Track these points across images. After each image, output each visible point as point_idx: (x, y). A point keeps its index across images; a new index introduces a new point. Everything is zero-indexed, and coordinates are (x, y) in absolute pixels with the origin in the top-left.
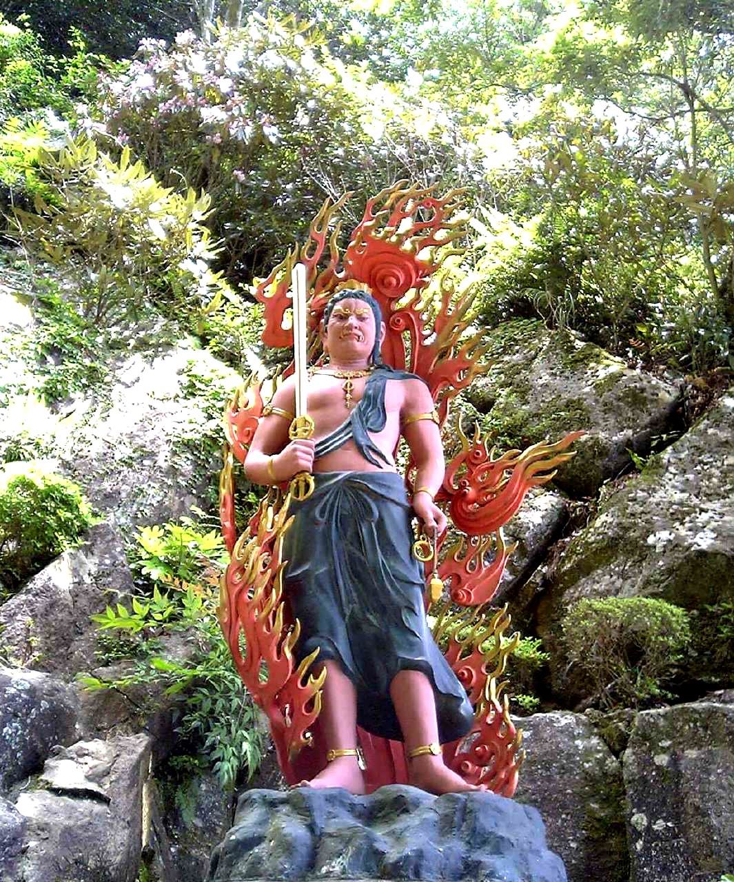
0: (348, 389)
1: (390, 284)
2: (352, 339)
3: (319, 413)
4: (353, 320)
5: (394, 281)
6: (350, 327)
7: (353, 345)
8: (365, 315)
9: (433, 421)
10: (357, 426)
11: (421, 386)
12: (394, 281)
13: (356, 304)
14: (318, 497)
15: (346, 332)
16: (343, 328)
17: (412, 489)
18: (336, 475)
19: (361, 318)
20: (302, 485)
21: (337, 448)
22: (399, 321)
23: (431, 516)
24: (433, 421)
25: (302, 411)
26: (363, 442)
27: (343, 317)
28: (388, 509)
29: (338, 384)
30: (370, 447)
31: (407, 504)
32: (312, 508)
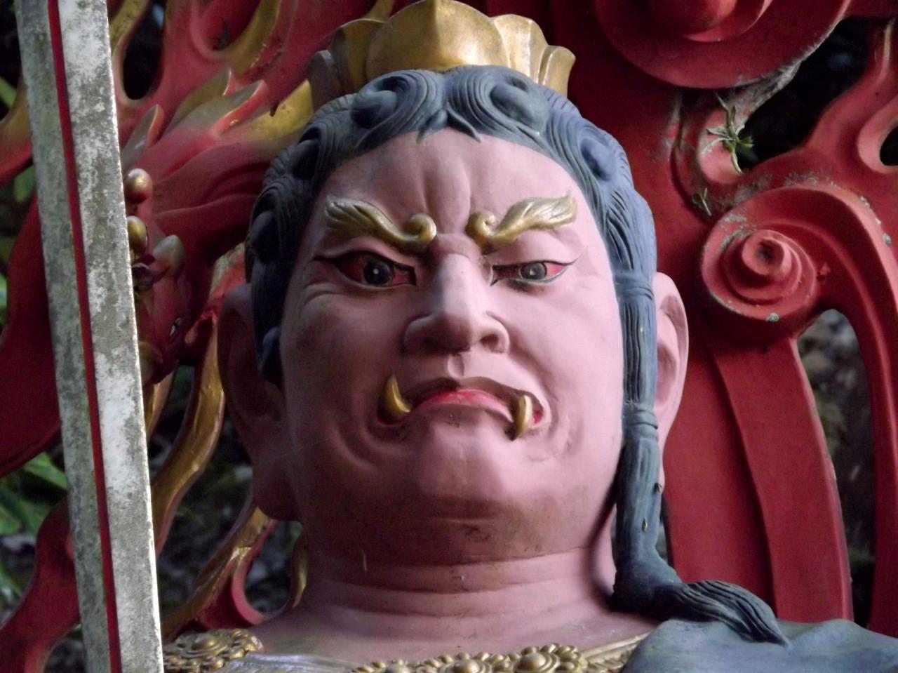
2: (465, 417)
7: (476, 464)
8: (546, 247)
13: (480, 172)
19: (515, 269)
22: (770, 253)
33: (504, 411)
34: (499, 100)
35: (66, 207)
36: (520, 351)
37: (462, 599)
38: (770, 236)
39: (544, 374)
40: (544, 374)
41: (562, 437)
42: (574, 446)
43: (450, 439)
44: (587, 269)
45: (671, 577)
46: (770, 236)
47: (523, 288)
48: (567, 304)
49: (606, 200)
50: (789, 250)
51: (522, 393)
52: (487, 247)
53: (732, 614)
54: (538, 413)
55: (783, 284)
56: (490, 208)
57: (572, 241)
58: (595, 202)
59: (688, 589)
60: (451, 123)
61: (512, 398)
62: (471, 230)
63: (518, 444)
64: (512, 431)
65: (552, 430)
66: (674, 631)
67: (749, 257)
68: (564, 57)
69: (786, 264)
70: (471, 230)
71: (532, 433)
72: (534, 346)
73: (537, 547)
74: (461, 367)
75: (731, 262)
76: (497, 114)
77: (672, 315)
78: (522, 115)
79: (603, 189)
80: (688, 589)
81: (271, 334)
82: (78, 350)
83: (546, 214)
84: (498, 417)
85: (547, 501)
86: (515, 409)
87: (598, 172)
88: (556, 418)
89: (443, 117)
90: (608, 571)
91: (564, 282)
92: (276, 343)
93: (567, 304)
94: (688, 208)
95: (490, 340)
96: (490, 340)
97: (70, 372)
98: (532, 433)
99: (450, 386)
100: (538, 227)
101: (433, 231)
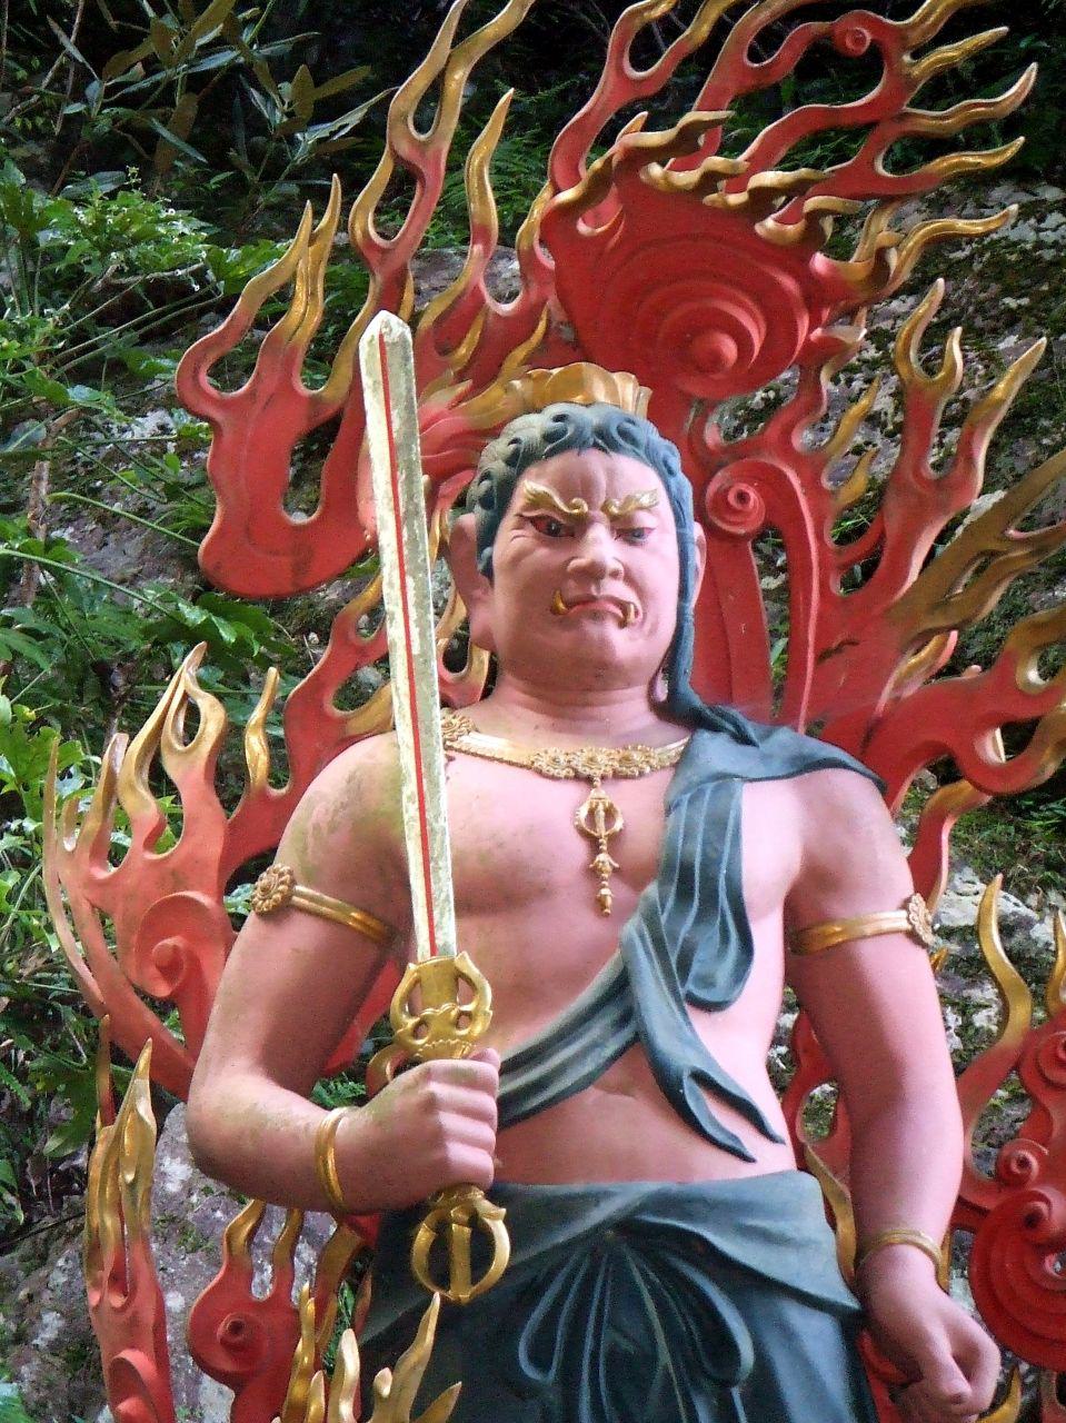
0: (601, 831)
1: (716, 358)
2: (598, 616)
3: (499, 931)
4: (601, 546)
5: (729, 348)
6: (594, 573)
7: (604, 643)
8: (644, 519)
9: (912, 935)
10: (786, 94)
11: (854, 789)
12: (729, 348)
13: (611, 474)
14: (524, 1286)
15: (573, 590)
16: (562, 573)
17: (864, 1263)
18: (595, 1198)
19: (628, 532)
20: (461, 1232)
21: (589, 1080)
22: (742, 497)
23: (943, 1349)
24: (912, 935)
25: (438, 930)
26: (682, 1058)
27: (561, 529)
28: (789, 1335)
29: (561, 806)
30: (702, 1079)
31: (851, 1303)
32: (508, 1333)
33: (621, 615)
34: (624, 434)
35: (390, 488)
36: (630, 579)
37: (588, 710)
38: (743, 487)
39: (640, 591)
40: (640, 591)
41: (647, 626)
42: (653, 631)
43: (592, 629)
44: (664, 530)
45: (697, 701)
46: (743, 487)
47: (632, 543)
48: (654, 551)
49: (674, 489)
50: (753, 495)
51: (629, 603)
52: (614, 519)
53: (731, 728)
54: (637, 613)
55: (749, 514)
56: (615, 495)
57: (658, 515)
58: (668, 488)
59: (708, 712)
60: (596, 445)
61: (624, 606)
62: (605, 508)
63: (625, 631)
64: (623, 624)
65: (643, 623)
66: (705, 736)
67: (731, 498)
68: (646, 392)
69: (751, 503)
70: (605, 508)
71: (633, 624)
72: (637, 577)
73: (629, 685)
74: (598, 589)
75: (722, 495)
76: (621, 441)
77: (700, 545)
78: (634, 441)
79: (672, 481)
80: (708, 712)
81: (487, 551)
82: (396, 573)
83: (645, 501)
84: (615, 616)
85: (637, 660)
86: (625, 611)
87: (671, 472)
88: (645, 614)
89: (591, 441)
90: (662, 692)
91: (652, 539)
92: (490, 558)
93: (654, 551)
94: (701, 466)
95: (615, 575)
96: (615, 575)
97: (391, 585)
98: (633, 624)
99: (593, 599)
100: (641, 508)
101: (586, 508)
